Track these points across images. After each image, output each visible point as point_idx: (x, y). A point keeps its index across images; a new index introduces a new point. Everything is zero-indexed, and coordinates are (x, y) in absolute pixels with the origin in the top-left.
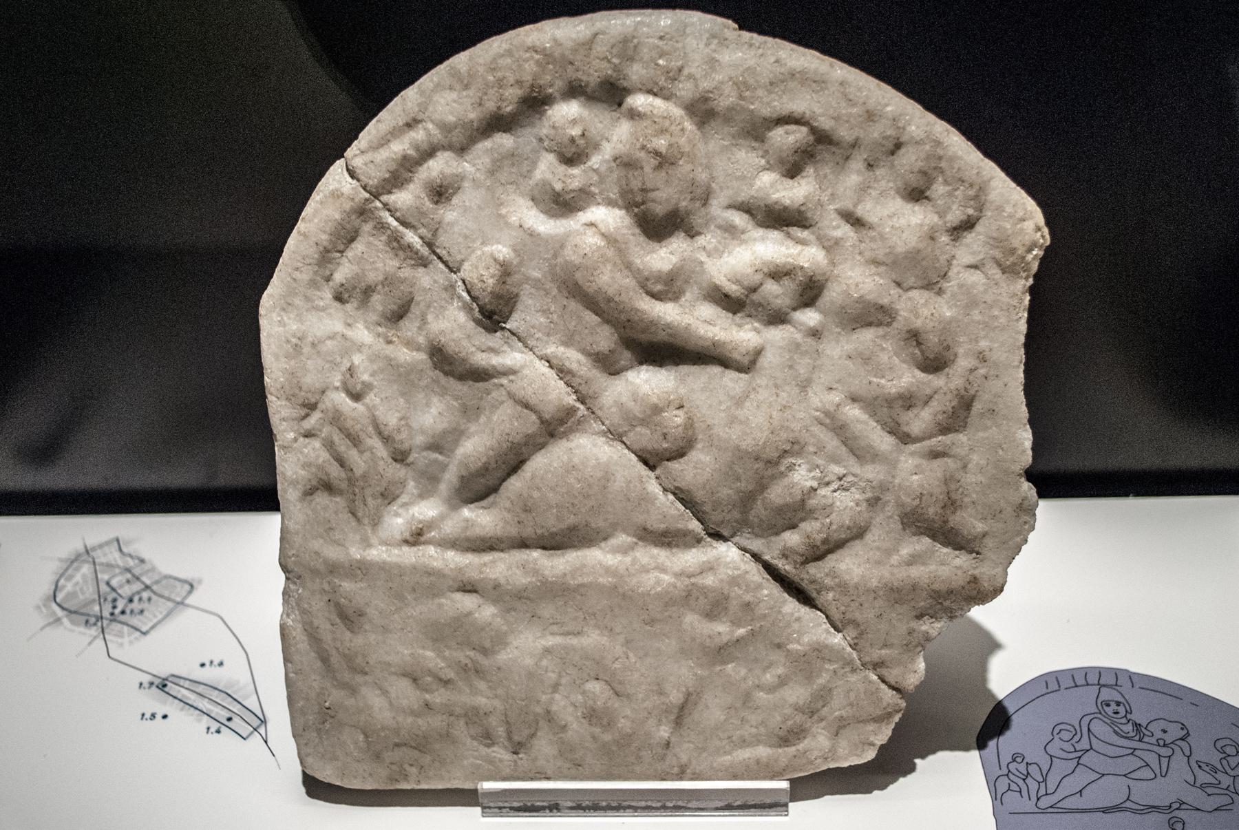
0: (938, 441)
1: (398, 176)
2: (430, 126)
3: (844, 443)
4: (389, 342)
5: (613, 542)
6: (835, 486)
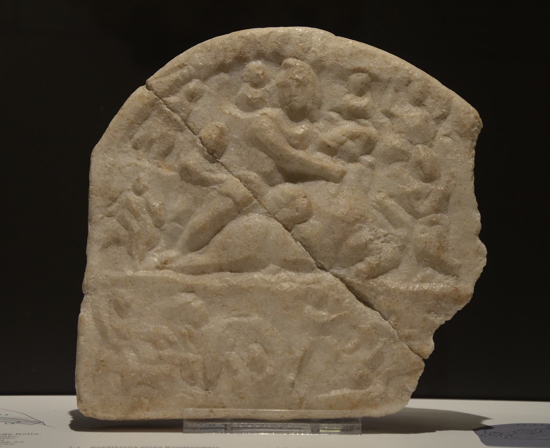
0: (433, 217)
1: (173, 89)
2: (191, 67)
3: (387, 218)
4: (160, 167)
5: (268, 269)
6: (382, 239)
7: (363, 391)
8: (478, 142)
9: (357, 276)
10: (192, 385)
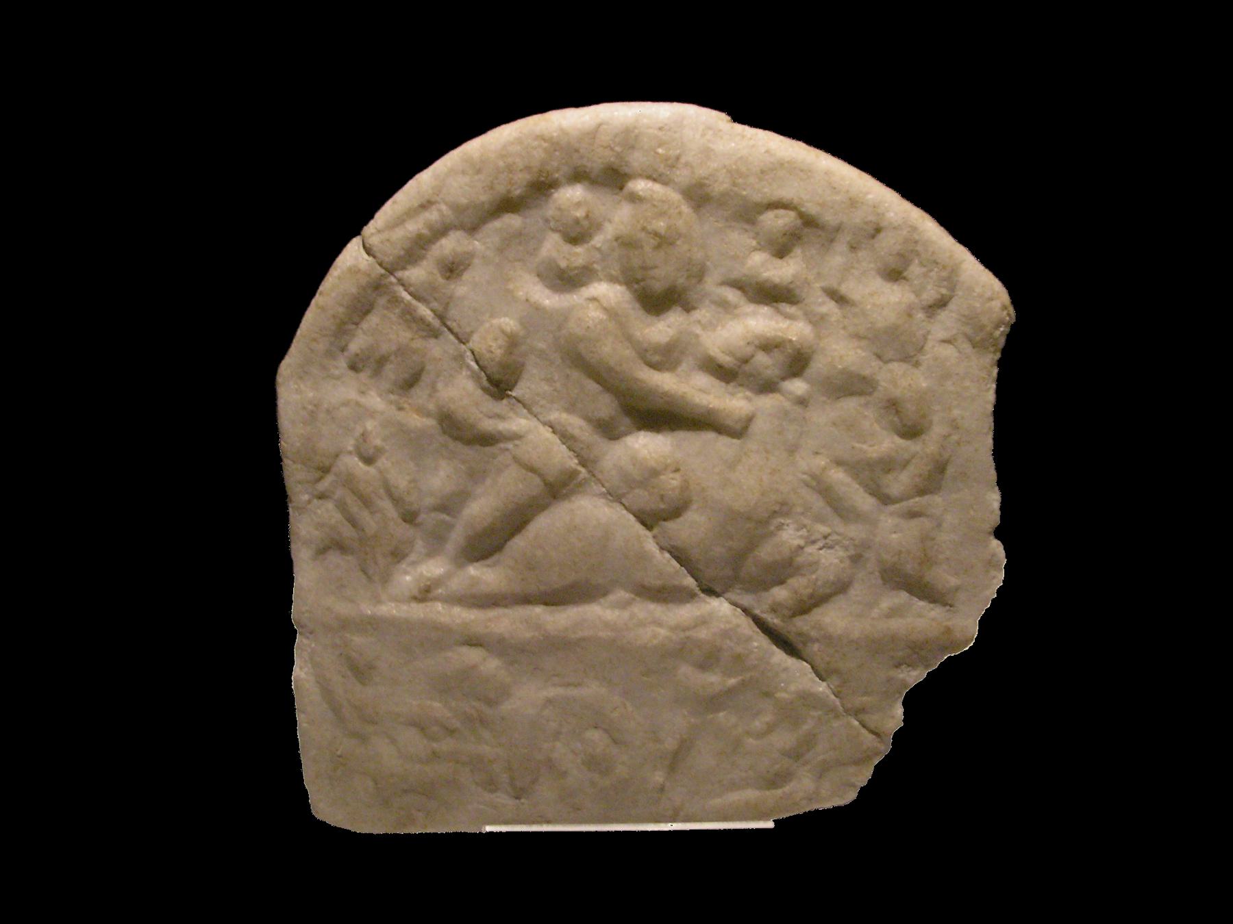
0: (916, 502)
1: (416, 249)
2: (444, 207)
4: (400, 409)
6: (820, 544)
7: (779, 792)
8: (1004, 351)
9: (774, 610)
10: (492, 791)
